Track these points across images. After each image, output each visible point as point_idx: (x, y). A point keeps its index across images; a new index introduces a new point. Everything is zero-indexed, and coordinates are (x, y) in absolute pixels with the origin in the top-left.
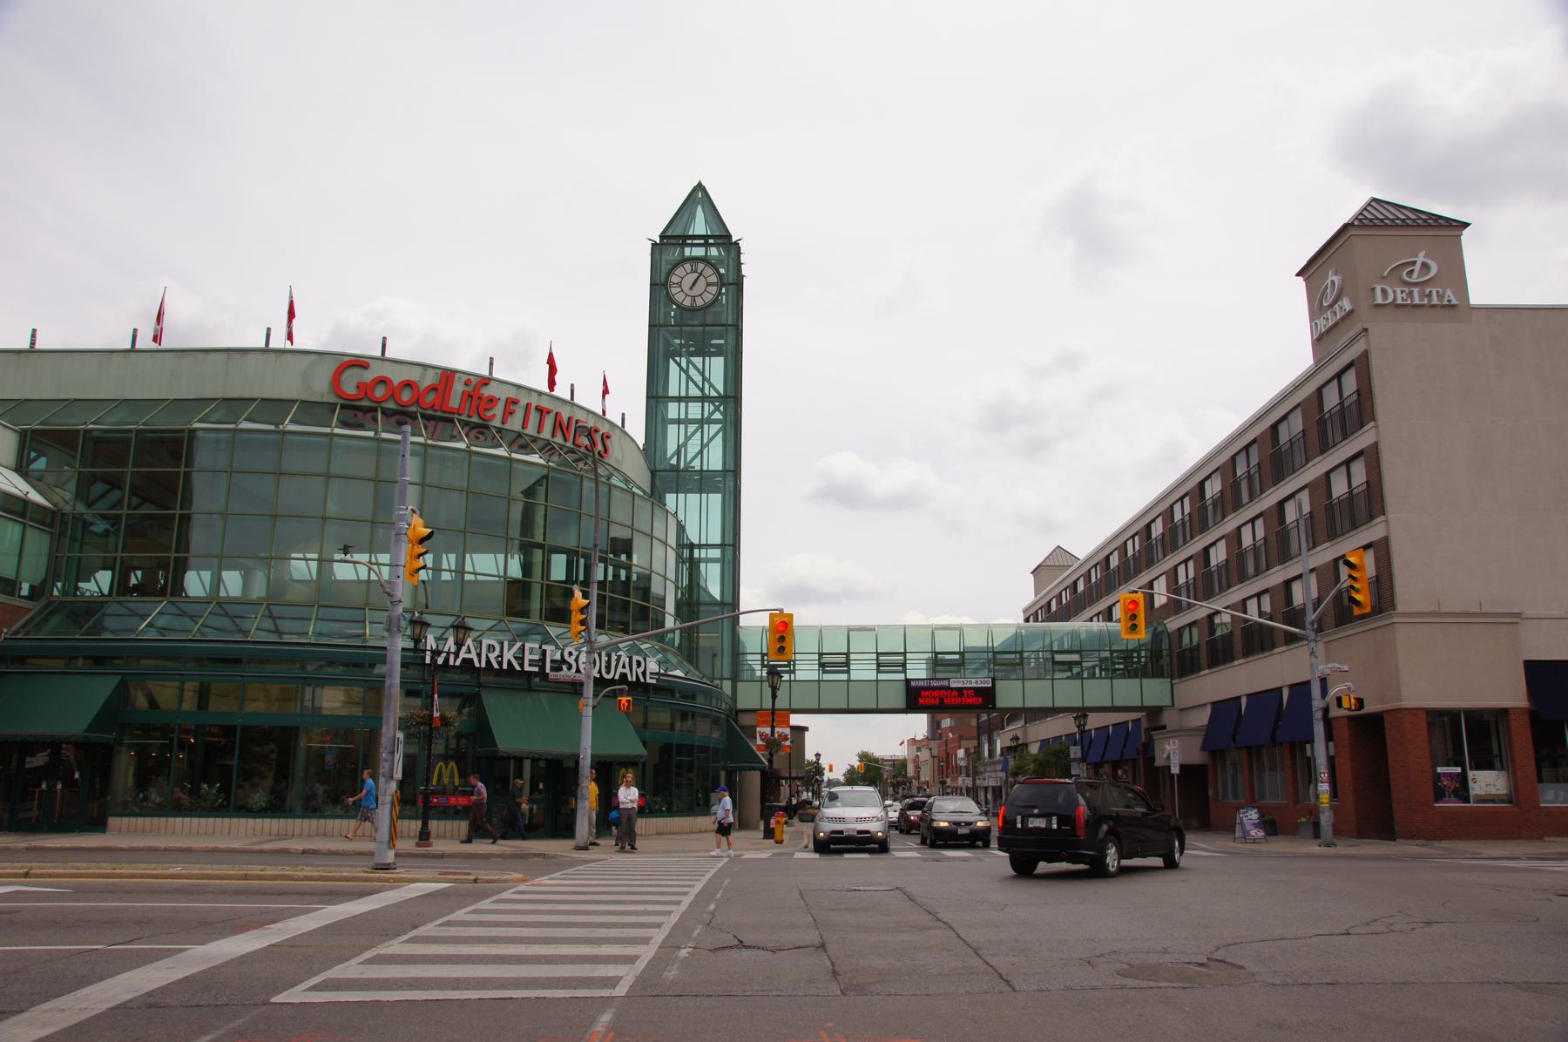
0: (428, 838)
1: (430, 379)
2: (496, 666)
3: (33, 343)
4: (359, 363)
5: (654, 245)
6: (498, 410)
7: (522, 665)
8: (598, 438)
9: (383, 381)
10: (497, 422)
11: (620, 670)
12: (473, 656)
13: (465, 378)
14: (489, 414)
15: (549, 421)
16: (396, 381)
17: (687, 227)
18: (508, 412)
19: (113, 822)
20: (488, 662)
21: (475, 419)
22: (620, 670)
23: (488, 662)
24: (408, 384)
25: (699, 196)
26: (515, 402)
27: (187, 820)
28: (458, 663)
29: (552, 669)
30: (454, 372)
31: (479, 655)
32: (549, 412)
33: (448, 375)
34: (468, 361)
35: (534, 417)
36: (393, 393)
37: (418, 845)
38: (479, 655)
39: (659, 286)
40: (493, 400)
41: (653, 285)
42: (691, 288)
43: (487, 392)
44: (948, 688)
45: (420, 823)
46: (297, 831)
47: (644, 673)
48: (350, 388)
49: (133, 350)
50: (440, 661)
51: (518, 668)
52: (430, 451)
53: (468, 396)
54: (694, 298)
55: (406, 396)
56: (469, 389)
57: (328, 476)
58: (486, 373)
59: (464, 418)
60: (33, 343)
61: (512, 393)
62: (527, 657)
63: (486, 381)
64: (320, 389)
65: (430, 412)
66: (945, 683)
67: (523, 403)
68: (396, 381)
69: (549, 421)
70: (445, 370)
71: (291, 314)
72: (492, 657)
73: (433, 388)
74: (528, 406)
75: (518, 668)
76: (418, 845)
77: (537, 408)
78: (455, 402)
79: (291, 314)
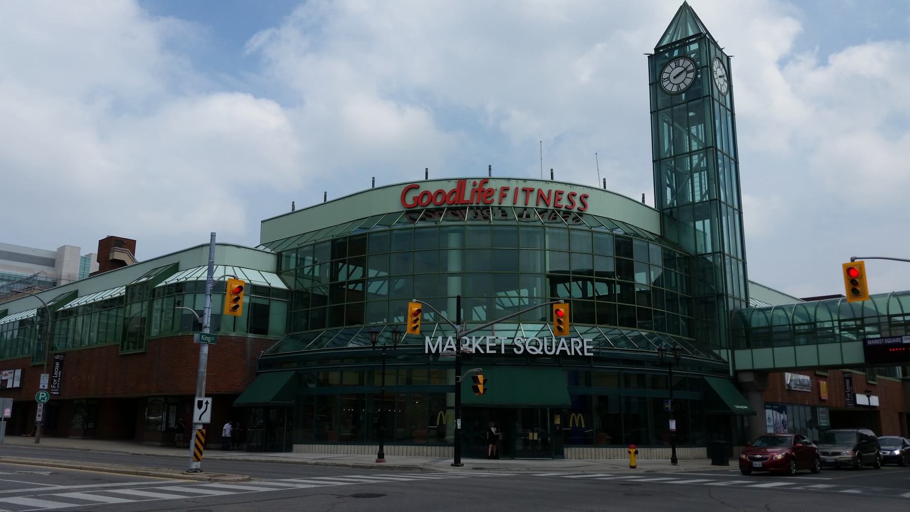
0: (383, 457)
3: (293, 209)
4: (413, 186)
5: (651, 57)
6: (496, 197)
7: (485, 350)
8: (577, 200)
9: (426, 193)
10: (495, 204)
11: (560, 348)
12: (566, 348)
13: (472, 181)
14: (489, 200)
15: (533, 198)
16: (447, 191)
19: (295, 446)
21: (481, 204)
24: (440, 192)
25: (686, 12)
26: (507, 189)
27: (397, 447)
29: (141, 347)
30: (465, 180)
31: (570, 348)
32: (532, 190)
33: (462, 182)
36: (432, 199)
38: (570, 348)
39: (656, 83)
40: (491, 191)
42: (677, 77)
43: (486, 187)
44: (901, 345)
45: (378, 447)
46: (429, 452)
47: (582, 349)
48: (410, 201)
49: (325, 203)
50: (433, 351)
51: (482, 352)
52: (572, 232)
53: (474, 191)
54: (678, 85)
55: (439, 199)
58: (487, 176)
60: (293, 209)
61: (505, 184)
62: (586, 347)
63: (485, 181)
64: (395, 206)
65: (454, 206)
66: (898, 340)
67: (512, 189)
68: (447, 191)
70: (459, 180)
71: (490, 169)
72: (578, 348)
73: (453, 192)
74: (517, 189)
75: (482, 352)
78: (467, 197)
79: (490, 169)
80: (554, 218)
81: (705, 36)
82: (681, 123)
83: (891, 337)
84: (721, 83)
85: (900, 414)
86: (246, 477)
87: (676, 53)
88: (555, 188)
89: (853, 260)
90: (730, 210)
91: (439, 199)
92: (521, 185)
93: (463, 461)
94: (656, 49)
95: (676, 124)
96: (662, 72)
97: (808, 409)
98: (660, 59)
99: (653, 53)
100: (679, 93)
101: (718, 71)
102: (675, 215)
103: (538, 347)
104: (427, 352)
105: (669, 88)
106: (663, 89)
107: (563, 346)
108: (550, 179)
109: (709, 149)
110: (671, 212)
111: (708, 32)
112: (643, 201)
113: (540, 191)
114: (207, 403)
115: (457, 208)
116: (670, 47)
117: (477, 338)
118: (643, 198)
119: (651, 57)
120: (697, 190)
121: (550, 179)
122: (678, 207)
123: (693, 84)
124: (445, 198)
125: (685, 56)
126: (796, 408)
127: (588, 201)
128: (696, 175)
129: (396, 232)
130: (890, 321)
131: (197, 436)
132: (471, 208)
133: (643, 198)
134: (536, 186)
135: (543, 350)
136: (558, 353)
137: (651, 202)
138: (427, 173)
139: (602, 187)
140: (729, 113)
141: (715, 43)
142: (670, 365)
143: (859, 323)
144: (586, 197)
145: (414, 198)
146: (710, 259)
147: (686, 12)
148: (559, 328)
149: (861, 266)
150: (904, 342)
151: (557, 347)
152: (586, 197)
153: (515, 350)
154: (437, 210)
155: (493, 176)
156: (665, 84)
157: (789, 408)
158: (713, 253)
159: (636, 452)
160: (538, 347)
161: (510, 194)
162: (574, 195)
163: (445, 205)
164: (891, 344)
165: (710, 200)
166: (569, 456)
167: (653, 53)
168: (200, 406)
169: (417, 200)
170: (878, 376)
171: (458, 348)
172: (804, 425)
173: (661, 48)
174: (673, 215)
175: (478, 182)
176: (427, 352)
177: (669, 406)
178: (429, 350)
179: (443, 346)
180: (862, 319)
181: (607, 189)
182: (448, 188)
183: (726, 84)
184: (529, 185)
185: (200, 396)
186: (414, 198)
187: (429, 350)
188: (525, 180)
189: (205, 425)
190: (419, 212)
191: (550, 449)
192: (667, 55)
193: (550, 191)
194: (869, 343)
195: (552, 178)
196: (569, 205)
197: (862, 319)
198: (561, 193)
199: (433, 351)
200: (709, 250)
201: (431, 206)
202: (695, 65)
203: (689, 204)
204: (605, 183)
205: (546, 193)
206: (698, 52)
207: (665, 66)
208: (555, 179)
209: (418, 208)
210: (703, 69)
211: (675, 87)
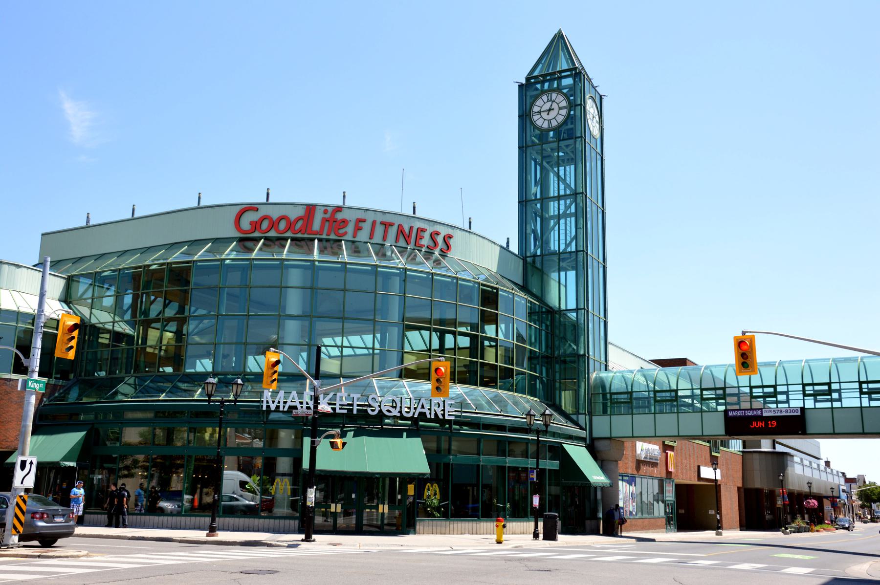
1: (301, 212)
2: (441, 417)
3: (88, 222)
5: (521, 86)
8: (440, 239)
13: (323, 209)
14: (341, 231)
15: (392, 232)
16: (275, 217)
17: (555, 66)
18: (358, 228)
20: (436, 414)
22: (419, 410)
23: (436, 414)
24: (281, 218)
25: (559, 42)
28: (286, 409)
31: (430, 409)
32: (392, 224)
33: (311, 209)
34: (326, 196)
35: (379, 230)
36: (274, 224)
37: (208, 535)
39: (525, 116)
40: (345, 222)
41: (520, 117)
42: (550, 112)
43: (339, 216)
48: (245, 224)
50: (273, 407)
53: (324, 220)
54: (550, 121)
56: (328, 216)
57: (345, 290)
58: (340, 203)
59: (324, 236)
61: (361, 215)
62: (447, 408)
63: (338, 209)
66: (758, 413)
68: (275, 217)
69: (392, 232)
71: (344, 196)
75: (441, 417)
76: (208, 535)
77: (382, 223)
78: (316, 226)
79: (344, 196)
80: (414, 259)
81: (580, 72)
82: (547, 162)
83: (751, 409)
84: (593, 126)
85: (739, 488)
86: (84, 552)
87: (546, 85)
88: (417, 225)
89: (744, 333)
90: (595, 264)
91: (282, 225)
92: (380, 218)
93: (314, 537)
94: (528, 79)
95: (545, 164)
96: (532, 104)
97: (656, 482)
98: (529, 90)
99: (524, 82)
100: (549, 130)
101: (591, 108)
102: (538, 265)
103: (395, 407)
104: (264, 408)
105: (539, 123)
106: (532, 123)
107: (423, 407)
108: (411, 214)
109: (577, 195)
110: (534, 262)
111: (583, 68)
112: (508, 246)
113: (400, 226)
114: (31, 463)
115: (303, 239)
116: (545, 78)
117: (326, 394)
118: (508, 243)
119: (521, 86)
120: (560, 238)
121: (411, 214)
122: (542, 255)
123: (565, 122)
124: (290, 225)
125: (559, 90)
126: (644, 480)
127: (451, 242)
128: (562, 221)
129: (227, 262)
130: (751, 392)
131: (18, 504)
132: (320, 240)
133: (508, 243)
134: (397, 221)
135: (400, 412)
136: (416, 416)
137: (514, 248)
138: (268, 194)
139: (467, 228)
140: (599, 157)
141: (590, 80)
142: (538, 432)
143: (721, 392)
144: (450, 237)
145: (251, 223)
146: (573, 315)
147: (559, 42)
148: (438, 388)
149: (752, 340)
150: (764, 415)
151: (415, 409)
152: (450, 237)
153: (369, 409)
154: (279, 239)
155: (347, 204)
156: (535, 118)
157: (638, 480)
158: (577, 310)
159: (504, 526)
160: (395, 407)
161: (366, 227)
162: (438, 234)
163: (289, 234)
164: (751, 416)
165: (577, 251)
166: (421, 531)
167: (524, 82)
168: (23, 467)
169: (256, 225)
170: (721, 448)
171: (316, 407)
172: (651, 499)
173: (533, 78)
174: (533, 266)
175: (330, 210)
176: (264, 408)
177: (535, 476)
178: (268, 407)
179: (285, 403)
180: (724, 389)
181: (473, 230)
182: (294, 214)
183: (598, 126)
184: (388, 219)
185: (23, 454)
186: (251, 223)
187: (268, 407)
188: (384, 213)
189: (27, 490)
190: (257, 240)
191: (403, 524)
192: (539, 86)
193: (411, 228)
194: (730, 414)
195: (470, 228)
196: (432, 244)
197: (724, 389)
198: (424, 230)
199: (273, 407)
200: (572, 305)
201: (272, 234)
202: (569, 101)
203: (554, 253)
204: (470, 223)
205: (407, 230)
206: (572, 88)
207: (536, 97)
208: (417, 215)
209: (256, 234)
210: (575, 105)
211: (546, 122)
